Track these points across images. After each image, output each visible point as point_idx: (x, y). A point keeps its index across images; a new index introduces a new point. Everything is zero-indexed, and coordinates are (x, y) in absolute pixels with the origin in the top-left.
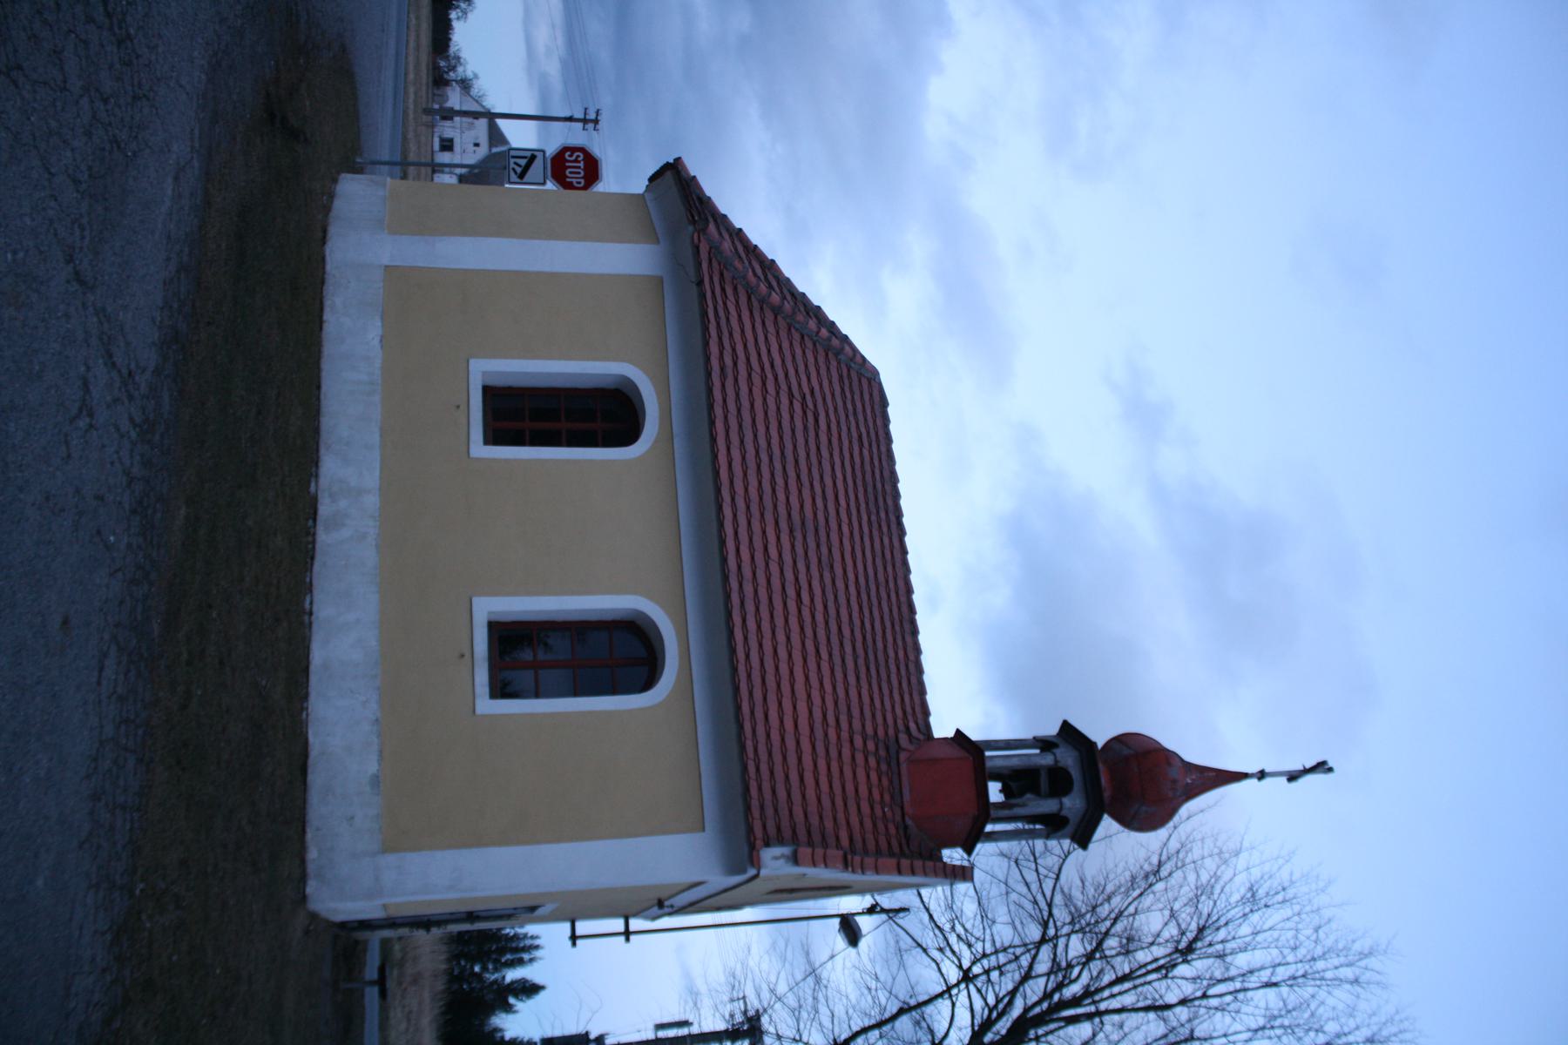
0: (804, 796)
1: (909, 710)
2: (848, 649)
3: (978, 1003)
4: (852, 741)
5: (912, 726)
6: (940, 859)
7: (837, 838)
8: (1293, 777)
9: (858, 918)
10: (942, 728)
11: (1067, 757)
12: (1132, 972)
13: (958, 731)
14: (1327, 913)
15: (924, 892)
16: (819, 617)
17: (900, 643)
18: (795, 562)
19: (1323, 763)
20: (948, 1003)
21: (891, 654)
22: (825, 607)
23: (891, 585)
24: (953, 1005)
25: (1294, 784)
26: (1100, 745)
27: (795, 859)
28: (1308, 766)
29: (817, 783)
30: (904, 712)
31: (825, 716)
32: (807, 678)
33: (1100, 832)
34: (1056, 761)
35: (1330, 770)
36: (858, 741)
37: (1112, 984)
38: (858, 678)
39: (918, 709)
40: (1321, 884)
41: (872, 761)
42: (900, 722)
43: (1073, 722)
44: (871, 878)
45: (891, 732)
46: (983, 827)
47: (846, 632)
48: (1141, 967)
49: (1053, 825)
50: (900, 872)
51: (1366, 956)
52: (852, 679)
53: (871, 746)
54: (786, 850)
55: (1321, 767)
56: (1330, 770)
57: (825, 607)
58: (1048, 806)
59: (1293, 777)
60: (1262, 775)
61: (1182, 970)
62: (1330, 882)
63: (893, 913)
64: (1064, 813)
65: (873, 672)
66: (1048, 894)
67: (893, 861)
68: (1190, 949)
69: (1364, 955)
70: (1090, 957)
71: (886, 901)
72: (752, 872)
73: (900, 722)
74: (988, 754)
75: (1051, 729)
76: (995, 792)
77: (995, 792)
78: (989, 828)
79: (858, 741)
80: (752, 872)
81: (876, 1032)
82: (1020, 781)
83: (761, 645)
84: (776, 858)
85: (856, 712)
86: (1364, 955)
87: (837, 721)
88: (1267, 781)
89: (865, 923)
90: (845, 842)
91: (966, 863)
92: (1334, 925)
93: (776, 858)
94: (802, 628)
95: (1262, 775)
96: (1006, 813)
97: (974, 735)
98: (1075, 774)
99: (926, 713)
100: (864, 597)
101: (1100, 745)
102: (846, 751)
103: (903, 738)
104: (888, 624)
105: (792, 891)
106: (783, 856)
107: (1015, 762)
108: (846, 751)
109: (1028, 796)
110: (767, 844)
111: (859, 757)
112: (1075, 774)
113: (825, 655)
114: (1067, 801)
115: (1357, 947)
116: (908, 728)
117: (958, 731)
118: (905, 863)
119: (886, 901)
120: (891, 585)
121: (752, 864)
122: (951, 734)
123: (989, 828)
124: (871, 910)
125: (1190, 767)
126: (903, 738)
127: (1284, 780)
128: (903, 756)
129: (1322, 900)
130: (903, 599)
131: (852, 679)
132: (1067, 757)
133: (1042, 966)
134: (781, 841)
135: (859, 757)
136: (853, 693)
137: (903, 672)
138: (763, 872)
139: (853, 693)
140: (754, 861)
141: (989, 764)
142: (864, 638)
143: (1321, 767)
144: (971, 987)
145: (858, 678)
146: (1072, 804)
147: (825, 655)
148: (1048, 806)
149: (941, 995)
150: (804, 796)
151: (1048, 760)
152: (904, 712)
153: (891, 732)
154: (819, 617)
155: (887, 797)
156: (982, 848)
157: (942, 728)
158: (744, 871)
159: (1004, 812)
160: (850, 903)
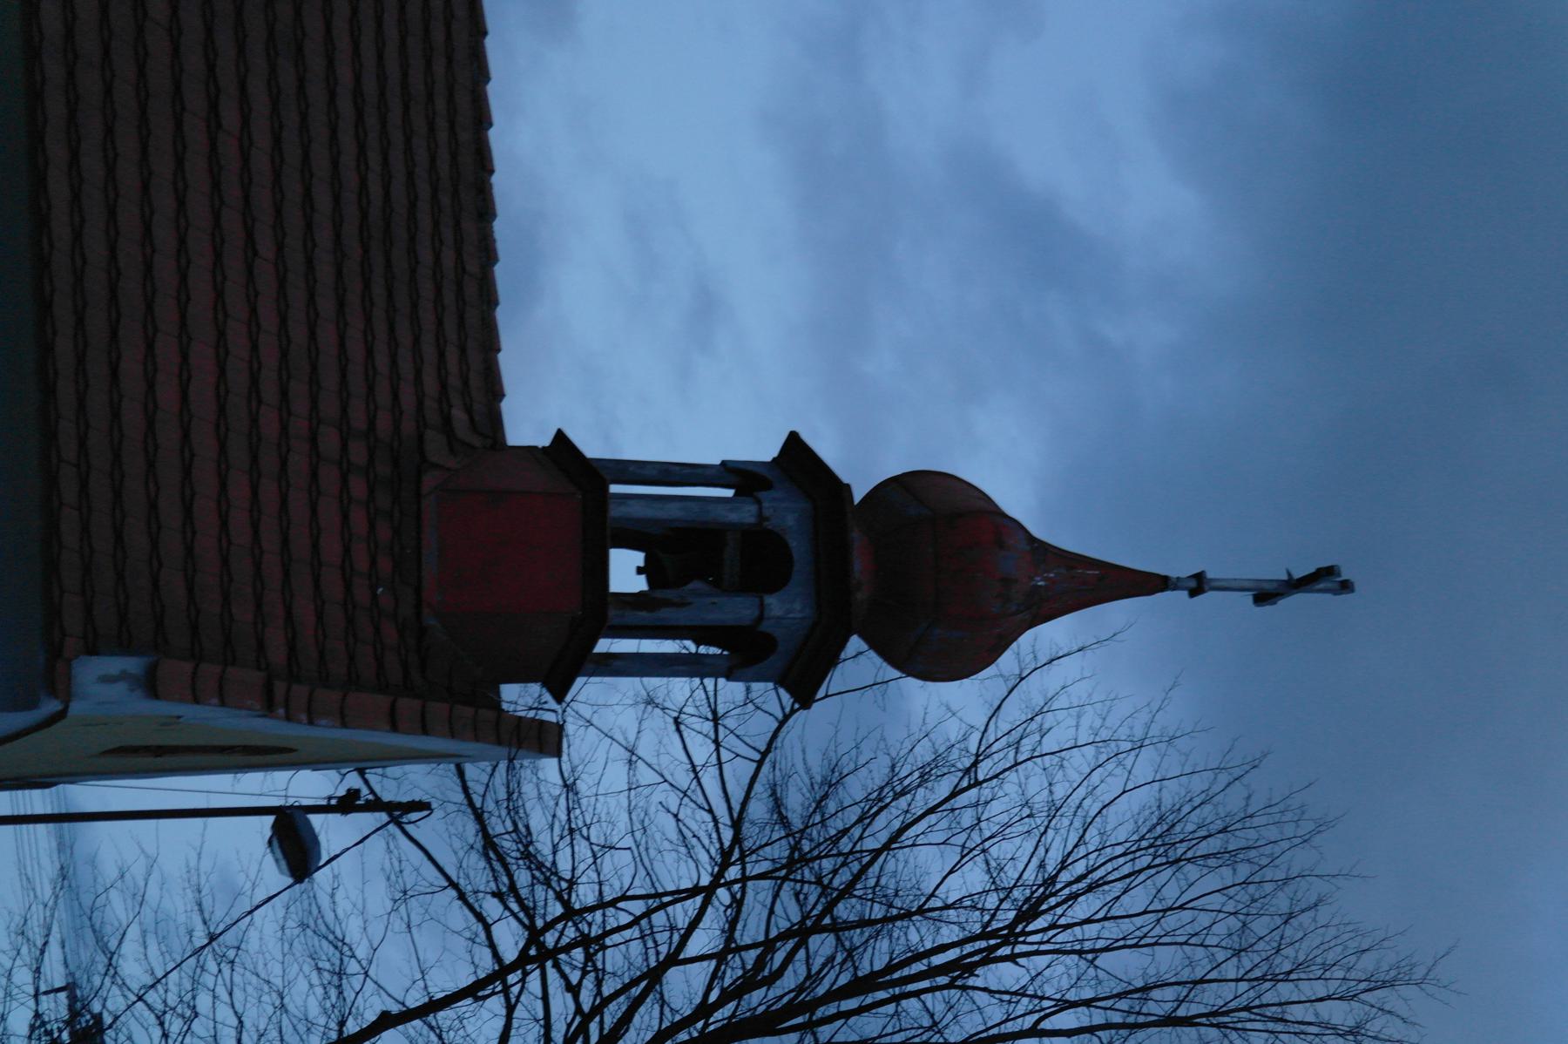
0: (190, 551)
1: (454, 381)
2: (324, 237)
3: (562, 1005)
4: (313, 440)
5: (458, 415)
6: (496, 704)
7: (261, 646)
8: (1264, 596)
9: (316, 820)
10: (526, 425)
11: (786, 514)
12: (890, 968)
13: (560, 437)
14: (1308, 891)
15: (471, 770)
16: (261, 162)
17: (448, 234)
18: (209, 30)
19: (1327, 572)
20: (496, 1004)
21: (426, 256)
22: (277, 141)
23: (440, 104)
24: (510, 1008)
25: (1268, 609)
26: (858, 497)
27: (151, 686)
28: (1298, 574)
29: (224, 524)
30: (443, 386)
31: (254, 381)
32: (219, 294)
33: (838, 679)
34: (761, 518)
35: (1346, 587)
36: (329, 441)
37: (835, 995)
38: (341, 304)
39: (475, 381)
40: (1307, 827)
41: (358, 487)
42: (430, 405)
43: (806, 437)
44: (327, 733)
45: (408, 426)
46: (594, 643)
47: (323, 201)
48: (918, 957)
49: (744, 653)
50: (394, 727)
51: (1384, 985)
52: (326, 306)
53: (358, 452)
54: (132, 665)
55: (1324, 579)
56: (1346, 587)
57: (277, 141)
58: (736, 610)
59: (1264, 596)
60: (1198, 585)
61: (990, 976)
62: (1321, 826)
63: (398, 812)
64: (765, 627)
65: (378, 291)
66: (737, 796)
67: (383, 701)
68: (1011, 935)
69: (1377, 984)
70: (800, 934)
71: (393, 783)
72: (51, 706)
73: (430, 405)
74: (615, 489)
75: (766, 450)
76: (625, 571)
77: (625, 571)
78: (604, 646)
79: (329, 441)
80: (51, 706)
81: (541, 1014)
82: (680, 549)
83: (112, 213)
84: (107, 679)
85: (330, 379)
86: (1377, 984)
87: (284, 393)
88: (1209, 597)
89: (331, 832)
90: (277, 652)
91: (550, 717)
92: (1323, 914)
93: (107, 679)
94: (216, 185)
95: (1198, 585)
96: (643, 617)
97: (592, 447)
98: (799, 547)
99: (495, 391)
100: (372, 121)
101: (858, 497)
102: (298, 461)
103: (435, 444)
104: (424, 189)
105: (160, 751)
106: (123, 676)
107: (673, 512)
108: (298, 461)
109: (696, 585)
110: (92, 651)
111: (329, 476)
112: (799, 547)
113: (266, 247)
114: (775, 604)
115: (1367, 963)
116: (447, 420)
117: (560, 437)
118: (408, 706)
119: (393, 783)
120: (440, 104)
121: (53, 692)
122: (544, 441)
123: (604, 646)
124: (347, 804)
125: (1042, 552)
126: (435, 444)
127: (1247, 598)
128: (430, 480)
129: (1300, 859)
130: (465, 136)
131: (326, 306)
132: (786, 514)
133: (704, 940)
134: (124, 645)
135: (329, 476)
136: (327, 337)
137: (449, 297)
138: (76, 708)
139: (327, 337)
140: (57, 682)
141: (615, 511)
142: (364, 215)
143: (1324, 579)
144: (552, 974)
145: (341, 304)
146: (786, 609)
147: (266, 247)
148: (736, 610)
149: (473, 991)
150: (190, 551)
151: (746, 514)
152: (443, 386)
153: (408, 426)
154: (261, 162)
155: (385, 565)
156: (588, 690)
157: (526, 425)
158: (31, 705)
159: (636, 615)
160: (308, 786)
